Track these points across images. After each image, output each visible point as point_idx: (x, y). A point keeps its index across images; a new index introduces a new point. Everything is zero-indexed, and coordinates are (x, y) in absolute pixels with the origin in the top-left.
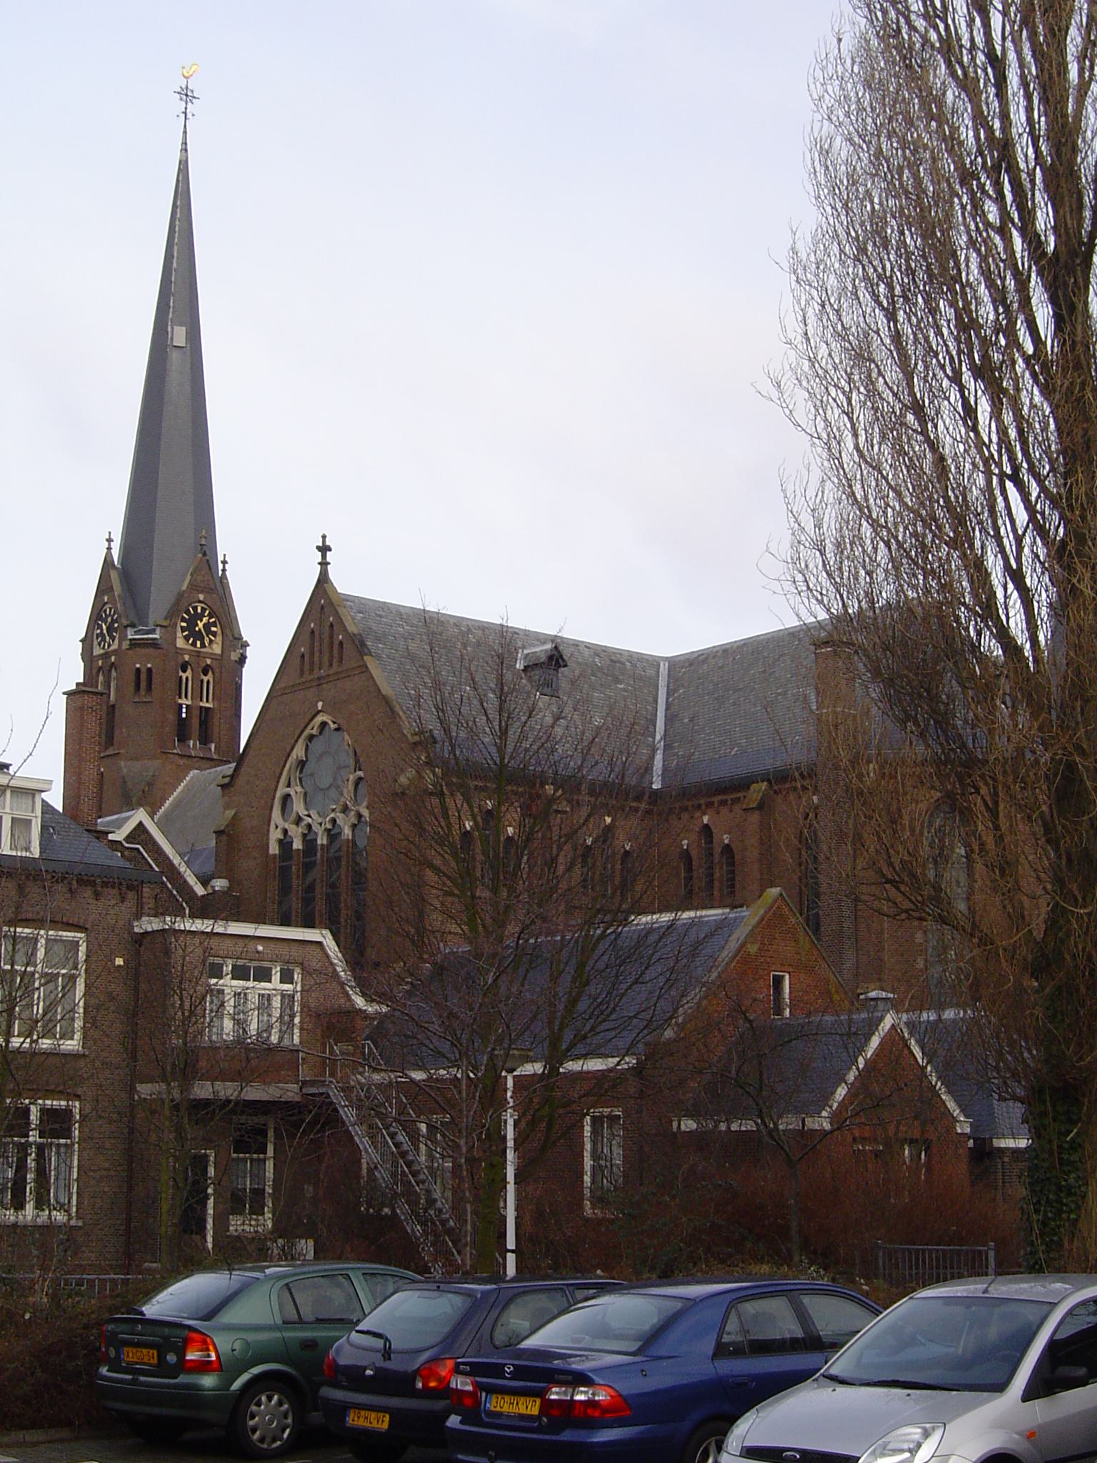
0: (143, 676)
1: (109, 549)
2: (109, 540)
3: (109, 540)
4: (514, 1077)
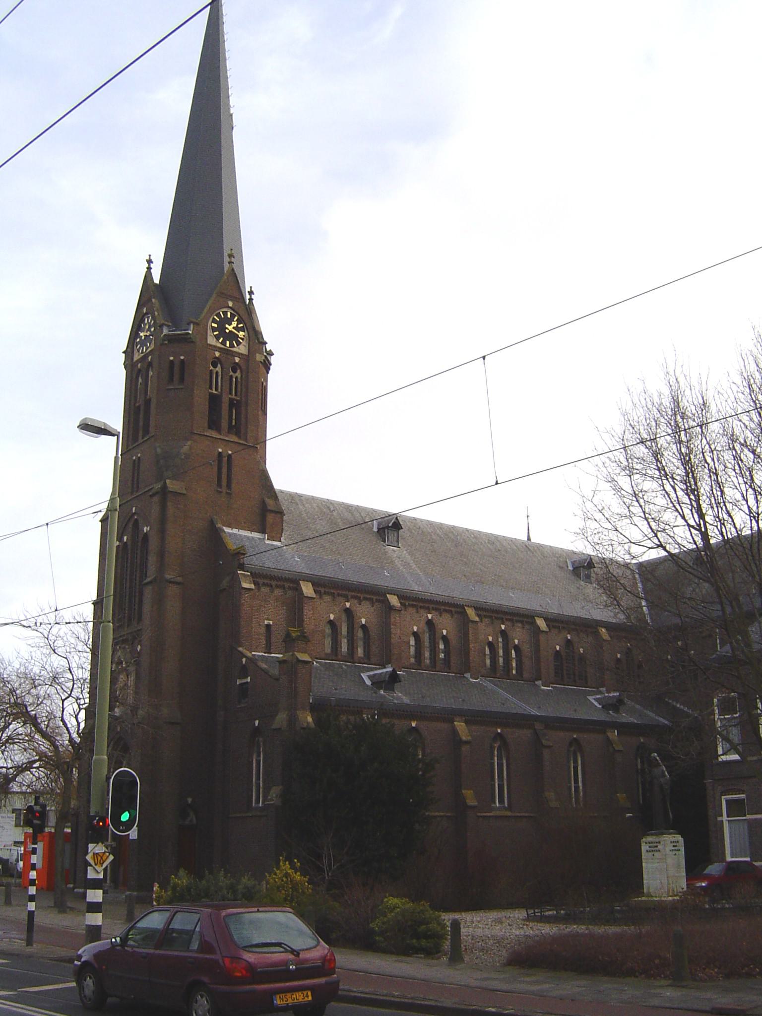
0: (176, 377)
1: (149, 268)
2: (149, 261)
3: (149, 261)
4: (723, 859)
